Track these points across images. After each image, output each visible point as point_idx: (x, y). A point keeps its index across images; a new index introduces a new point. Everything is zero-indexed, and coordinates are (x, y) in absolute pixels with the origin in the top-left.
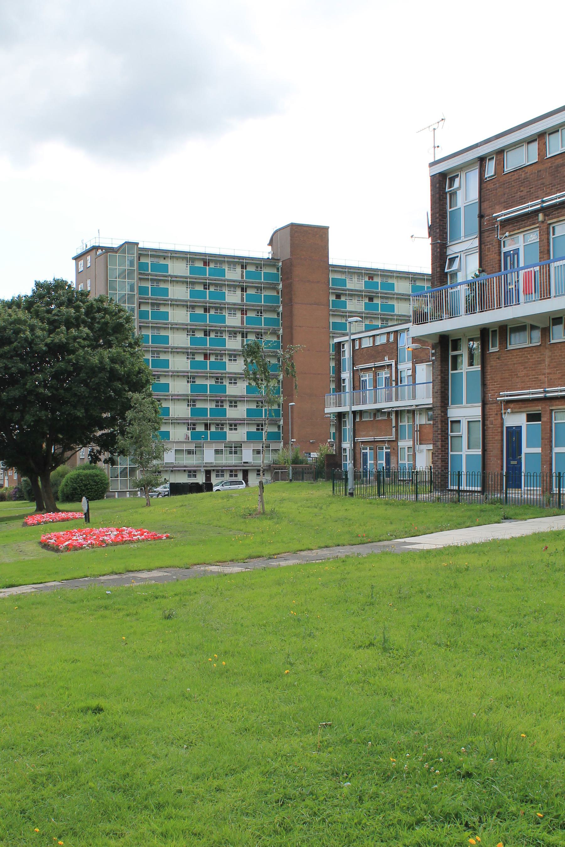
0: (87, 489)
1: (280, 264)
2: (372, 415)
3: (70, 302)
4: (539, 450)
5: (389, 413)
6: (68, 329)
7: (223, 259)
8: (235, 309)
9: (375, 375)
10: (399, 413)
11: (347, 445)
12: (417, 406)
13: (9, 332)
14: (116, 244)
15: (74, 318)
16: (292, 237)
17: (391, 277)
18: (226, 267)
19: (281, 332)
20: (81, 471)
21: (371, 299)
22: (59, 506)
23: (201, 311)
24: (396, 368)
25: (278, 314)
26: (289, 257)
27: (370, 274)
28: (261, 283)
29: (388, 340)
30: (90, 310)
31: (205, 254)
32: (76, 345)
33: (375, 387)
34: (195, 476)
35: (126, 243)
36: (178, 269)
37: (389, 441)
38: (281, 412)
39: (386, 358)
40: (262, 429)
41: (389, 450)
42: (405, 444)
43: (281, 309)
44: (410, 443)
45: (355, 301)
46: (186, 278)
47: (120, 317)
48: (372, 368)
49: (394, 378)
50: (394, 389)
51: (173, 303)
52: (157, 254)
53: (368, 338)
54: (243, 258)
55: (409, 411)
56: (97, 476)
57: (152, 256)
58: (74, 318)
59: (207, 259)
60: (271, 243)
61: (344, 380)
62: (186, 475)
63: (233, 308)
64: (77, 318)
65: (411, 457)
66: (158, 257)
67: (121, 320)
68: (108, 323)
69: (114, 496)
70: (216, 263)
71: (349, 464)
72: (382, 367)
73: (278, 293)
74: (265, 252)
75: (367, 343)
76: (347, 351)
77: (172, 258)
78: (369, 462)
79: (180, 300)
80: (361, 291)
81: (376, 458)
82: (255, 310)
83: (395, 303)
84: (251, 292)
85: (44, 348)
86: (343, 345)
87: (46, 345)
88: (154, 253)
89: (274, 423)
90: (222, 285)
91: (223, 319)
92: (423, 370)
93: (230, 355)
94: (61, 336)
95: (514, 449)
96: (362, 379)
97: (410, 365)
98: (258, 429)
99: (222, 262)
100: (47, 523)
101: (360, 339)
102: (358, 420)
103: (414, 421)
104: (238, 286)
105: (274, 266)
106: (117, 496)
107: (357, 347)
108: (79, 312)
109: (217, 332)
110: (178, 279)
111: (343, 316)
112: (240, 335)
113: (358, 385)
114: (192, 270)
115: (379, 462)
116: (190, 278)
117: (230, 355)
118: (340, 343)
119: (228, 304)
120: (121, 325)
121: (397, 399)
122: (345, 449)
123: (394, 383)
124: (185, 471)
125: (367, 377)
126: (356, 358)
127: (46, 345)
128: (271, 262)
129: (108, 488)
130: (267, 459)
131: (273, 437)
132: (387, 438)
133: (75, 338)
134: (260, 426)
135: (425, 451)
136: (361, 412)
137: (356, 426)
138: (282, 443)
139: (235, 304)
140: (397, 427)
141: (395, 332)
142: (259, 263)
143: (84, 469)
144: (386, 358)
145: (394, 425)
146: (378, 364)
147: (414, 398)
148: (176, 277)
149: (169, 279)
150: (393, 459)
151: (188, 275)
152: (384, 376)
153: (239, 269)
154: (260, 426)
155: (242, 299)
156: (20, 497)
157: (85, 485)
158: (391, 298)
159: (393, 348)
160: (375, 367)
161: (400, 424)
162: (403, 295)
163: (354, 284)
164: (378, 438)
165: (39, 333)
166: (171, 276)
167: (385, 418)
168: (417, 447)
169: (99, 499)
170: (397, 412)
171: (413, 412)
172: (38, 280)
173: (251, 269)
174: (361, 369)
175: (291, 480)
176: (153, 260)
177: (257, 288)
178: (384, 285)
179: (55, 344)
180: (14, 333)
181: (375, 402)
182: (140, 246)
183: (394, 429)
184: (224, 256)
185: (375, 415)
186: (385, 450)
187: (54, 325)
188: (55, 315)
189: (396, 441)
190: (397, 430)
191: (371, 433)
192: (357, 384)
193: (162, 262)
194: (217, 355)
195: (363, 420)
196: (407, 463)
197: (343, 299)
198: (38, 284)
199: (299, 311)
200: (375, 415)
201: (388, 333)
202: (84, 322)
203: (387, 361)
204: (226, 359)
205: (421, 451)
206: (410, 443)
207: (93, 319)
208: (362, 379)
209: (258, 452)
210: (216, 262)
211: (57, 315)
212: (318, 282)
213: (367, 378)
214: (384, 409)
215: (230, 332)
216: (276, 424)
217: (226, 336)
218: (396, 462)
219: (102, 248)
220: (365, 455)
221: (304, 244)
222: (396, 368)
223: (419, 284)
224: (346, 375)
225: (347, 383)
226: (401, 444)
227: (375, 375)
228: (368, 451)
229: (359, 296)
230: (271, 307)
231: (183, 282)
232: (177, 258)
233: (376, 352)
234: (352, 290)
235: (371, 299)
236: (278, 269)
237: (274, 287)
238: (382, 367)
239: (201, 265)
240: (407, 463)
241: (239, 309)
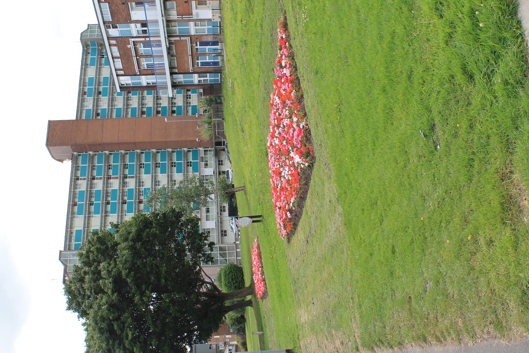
0: (235, 278)
1: (75, 153)
2: (172, 58)
3: (82, 280)
4: (207, 52)
5: (170, 43)
6: (101, 278)
7: (72, 193)
8: (107, 184)
9: (142, 56)
10: (170, 35)
11: (196, 79)
12: (162, 16)
13: (104, 325)
14: (62, 267)
15: (94, 276)
16: (55, 145)
17: (84, 79)
18: (78, 190)
19: (123, 152)
20: (222, 284)
21: (100, 93)
22: (247, 284)
23: (109, 207)
24: (136, 37)
25: (110, 154)
26: (70, 147)
27: (82, 94)
28: (89, 166)
29: (115, 45)
30: (87, 263)
31: (69, 205)
32: (114, 270)
33: (151, 56)
34: (224, 207)
35: (60, 259)
36: (79, 223)
37: (191, 43)
38: (178, 150)
39: (129, 46)
40: (191, 162)
41: (198, 43)
42: (192, 29)
43: (107, 152)
44: (192, 24)
45: (101, 103)
46: (85, 217)
47: (93, 240)
48: (137, 59)
49: (143, 39)
50: (152, 39)
51: (103, 225)
52: (68, 237)
53: (115, 63)
54: (71, 179)
55: (168, 26)
56: (226, 272)
57: (70, 241)
58: (94, 276)
59: (72, 204)
60: (61, 161)
61: (148, 84)
62: (223, 213)
63: (107, 184)
64: (94, 273)
65: (203, 23)
66: (71, 237)
67: (95, 238)
68: (97, 249)
69: (240, 260)
70: (75, 197)
71: (209, 78)
72: (136, 50)
73: (96, 154)
74: (68, 164)
75: (119, 64)
76: (126, 80)
77: (71, 228)
78: (208, 61)
79: (101, 221)
80: (94, 99)
81: (204, 54)
82: (108, 171)
83: (102, 77)
84: (95, 173)
85: (115, 295)
86: (122, 85)
87: (113, 294)
88: (68, 240)
89: (186, 154)
90: (91, 193)
91: (114, 191)
92: (135, 14)
93: (140, 186)
94: (107, 283)
95: (208, 64)
96: (146, 68)
97: (133, 25)
98: (191, 166)
99: (74, 194)
100: (263, 273)
101: (116, 70)
102: (176, 71)
103: (174, 21)
104: (91, 182)
105: (77, 158)
106: (240, 258)
107: (122, 72)
108: (89, 272)
109: (123, 196)
110: (86, 223)
111: (112, 111)
112: (126, 179)
113: (150, 71)
114: (80, 213)
115: (207, 52)
116: (85, 214)
117: (140, 186)
118: (120, 87)
119: (103, 188)
120: (99, 238)
121: (159, 36)
122: (199, 81)
123: (147, 39)
124: (221, 214)
125: (144, 63)
126: (131, 73)
127: (113, 294)
128: (74, 160)
129: (235, 266)
130: (212, 160)
131: (196, 154)
132: (189, 44)
133: (109, 272)
134: (189, 164)
135: (197, 11)
136: (171, 68)
137: (181, 72)
138: (200, 148)
139: (104, 184)
140: (180, 36)
141: (108, 40)
142: (75, 168)
143: (221, 282)
144: (129, 46)
145: (178, 38)
146: (134, 54)
147: (156, 22)
148: (85, 224)
149: (86, 229)
150: (205, 39)
151: (83, 216)
152: (143, 49)
153: (79, 182)
154: (189, 164)
155: (100, 178)
156: (243, 331)
157: (233, 280)
158: (99, 79)
159: (121, 41)
160: (136, 56)
161: (178, 34)
162: (96, 72)
163: (89, 104)
164: (190, 52)
165: (104, 300)
166: (84, 227)
167: (174, 46)
168: (195, 18)
169: (242, 270)
170: (169, 36)
171: (168, 21)
172: (66, 308)
173: (79, 173)
174: (139, 68)
175: (223, 119)
176: (73, 241)
177: (93, 169)
178: (90, 84)
179: (114, 287)
180: (104, 322)
181: (162, 56)
182: (63, 250)
183: (182, 38)
184: (70, 192)
185: (172, 56)
186: (198, 47)
187: (99, 291)
188: (91, 293)
189: (191, 36)
190: (183, 36)
191: (186, 59)
192: (150, 72)
193: (74, 234)
194: (139, 195)
195: (176, 66)
196: (206, 27)
197: (99, 111)
198: (69, 308)
199: (108, 138)
200: (172, 56)
201: (110, 45)
202: (96, 268)
203: (131, 46)
204: (142, 189)
205: (197, 14)
206: (192, 24)
207: (94, 260)
208: (146, 68)
209: (206, 165)
210: (74, 197)
211: (91, 290)
212: (87, 126)
213: (145, 63)
214: (167, 46)
215: (123, 186)
216: (187, 154)
217: (126, 189)
218: (207, 37)
219: (64, 277)
220: (203, 64)
221: (61, 137)
222: (136, 37)
223: (89, 62)
224: (144, 80)
225: (150, 81)
226: (193, 33)
227: (142, 56)
228: (199, 61)
229: (98, 101)
230: (105, 159)
231: (89, 220)
232: (72, 224)
233: (125, 56)
234: (94, 105)
235: (100, 93)
236: (79, 155)
237: (92, 158)
238: (136, 50)
239: (76, 208)
240: (206, 27)
241: (107, 181)
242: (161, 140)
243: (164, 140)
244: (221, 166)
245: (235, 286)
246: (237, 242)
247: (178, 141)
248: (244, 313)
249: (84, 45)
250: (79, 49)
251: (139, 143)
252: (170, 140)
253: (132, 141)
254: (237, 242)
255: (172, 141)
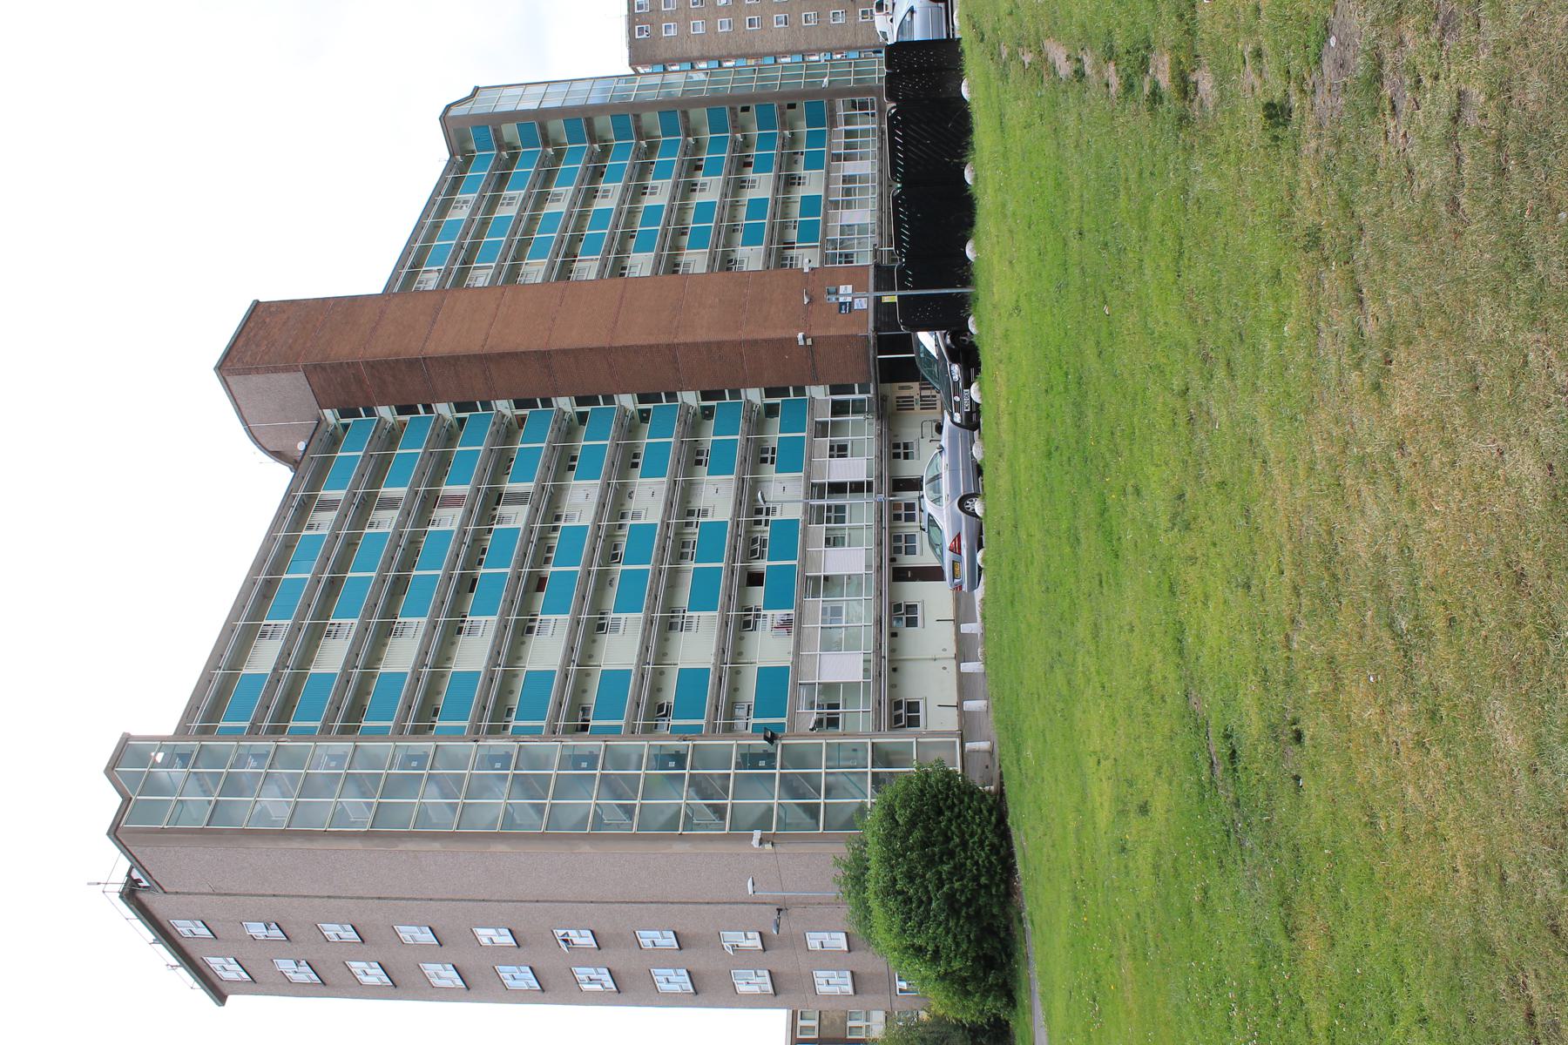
14: (117, 800)
16: (247, 371)
26: (301, 375)
116: (302, 615)
124: (894, 635)
130: (863, 433)
242: (652, 340)
243: (664, 339)
244: (902, 461)
245: (950, 898)
246: (970, 705)
247: (720, 344)
248: (1011, 1000)
249: (455, 144)
250: (435, 155)
251: (564, 352)
252: (689, 339)
253: (537, 345)
254: (970, 705)
255: (696, 344)
